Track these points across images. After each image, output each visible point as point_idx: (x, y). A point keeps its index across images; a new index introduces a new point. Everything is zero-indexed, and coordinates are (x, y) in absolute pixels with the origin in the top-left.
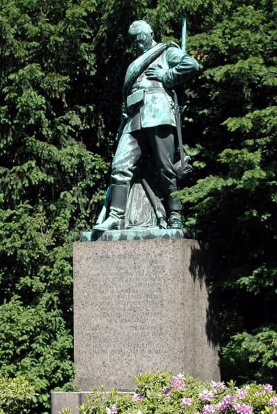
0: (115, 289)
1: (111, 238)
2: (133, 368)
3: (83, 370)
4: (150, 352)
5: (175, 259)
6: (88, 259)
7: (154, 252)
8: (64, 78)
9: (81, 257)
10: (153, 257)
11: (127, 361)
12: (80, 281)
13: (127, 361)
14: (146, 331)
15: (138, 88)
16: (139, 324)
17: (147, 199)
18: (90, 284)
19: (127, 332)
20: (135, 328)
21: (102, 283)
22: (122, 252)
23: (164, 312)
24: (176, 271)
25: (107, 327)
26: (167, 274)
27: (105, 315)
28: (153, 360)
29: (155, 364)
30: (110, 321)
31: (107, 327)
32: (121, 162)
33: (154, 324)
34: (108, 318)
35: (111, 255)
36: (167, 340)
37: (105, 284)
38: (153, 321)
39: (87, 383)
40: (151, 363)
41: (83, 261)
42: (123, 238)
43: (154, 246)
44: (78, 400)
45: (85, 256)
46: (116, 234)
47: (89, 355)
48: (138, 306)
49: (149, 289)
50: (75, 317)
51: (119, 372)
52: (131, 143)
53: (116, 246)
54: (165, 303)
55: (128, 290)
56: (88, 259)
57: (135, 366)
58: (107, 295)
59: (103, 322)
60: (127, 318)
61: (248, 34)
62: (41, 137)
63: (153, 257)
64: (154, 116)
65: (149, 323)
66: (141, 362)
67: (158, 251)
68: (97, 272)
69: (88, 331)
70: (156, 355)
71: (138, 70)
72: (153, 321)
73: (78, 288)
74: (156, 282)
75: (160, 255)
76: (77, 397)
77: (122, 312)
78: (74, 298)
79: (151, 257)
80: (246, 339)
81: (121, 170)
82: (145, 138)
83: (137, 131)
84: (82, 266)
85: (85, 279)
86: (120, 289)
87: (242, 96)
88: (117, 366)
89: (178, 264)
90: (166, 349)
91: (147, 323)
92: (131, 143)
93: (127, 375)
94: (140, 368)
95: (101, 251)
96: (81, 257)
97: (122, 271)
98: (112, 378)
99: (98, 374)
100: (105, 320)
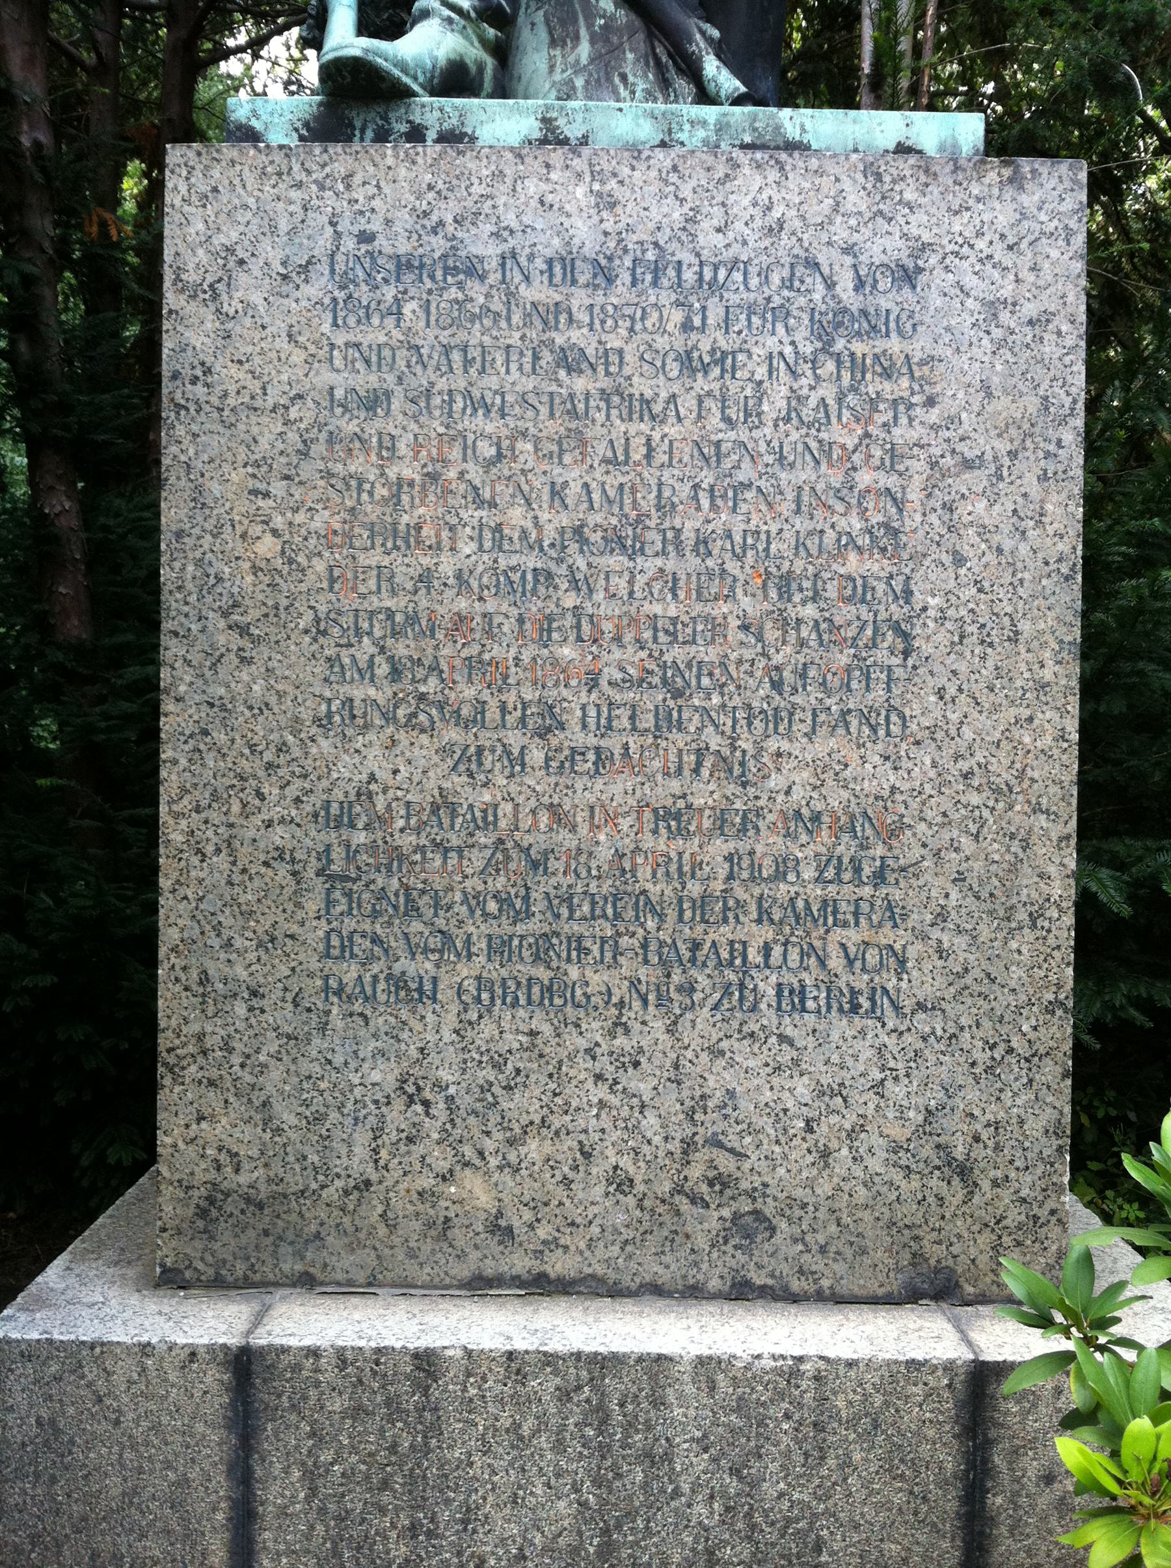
0: (517, 516)
2: (650, 1122)
3: (230, 1128)
4: (794, 999)
5: (1030, 309)
7: (848, 250)
8: (389, 152)
9: (233, 260)
11: (604, 1064)
12: (215, 444)
13: (604, 1064)
14: (768, 844)
18: (308, 470)
21: (410, 471)
22: (585, 233)
23: (923, 708)
24: (1032, 404)
25: (444, 804)
26: (953, 420)
27: (416, 714)
28: (814, 1061)
29: (839, 1091)
30: (469, 762)
31: (444, 804)
33: (837, 797)
34: (453, 734)
35: (491, 251)
36: (942, 916)
37: (433, 477)
40: (803, 1088)
41: (250, 289)
43: (855, 200)
45: (272, 252)
47: (286, 1017)
48: (711, 654)
51: (534, 1149)
53: (532, 187)
54: (932, 640)
57: (670, 1101)
58: (447, 566)
60: (613, 743)
66: (720, 1078)
69: (279, 836)
70: (840, 1027)
73: (199, 500)
74: (864, 478)
75: (907, 276)
76: (214, 1378)
77: (574, 701)
79: (830, 285)
86: (553, 521)
87: (544, 1385)
88: (524, 1104)
89: (1049, 349)
90: (925, 981)
91: (775, 781)
93: (599, 1169)
94: (711, 1123)
95: (404, 220)
96: (233, 260)
97: (580, 384)
98: (477, 1192)
99: (358, 1162)
100: (423, 749)
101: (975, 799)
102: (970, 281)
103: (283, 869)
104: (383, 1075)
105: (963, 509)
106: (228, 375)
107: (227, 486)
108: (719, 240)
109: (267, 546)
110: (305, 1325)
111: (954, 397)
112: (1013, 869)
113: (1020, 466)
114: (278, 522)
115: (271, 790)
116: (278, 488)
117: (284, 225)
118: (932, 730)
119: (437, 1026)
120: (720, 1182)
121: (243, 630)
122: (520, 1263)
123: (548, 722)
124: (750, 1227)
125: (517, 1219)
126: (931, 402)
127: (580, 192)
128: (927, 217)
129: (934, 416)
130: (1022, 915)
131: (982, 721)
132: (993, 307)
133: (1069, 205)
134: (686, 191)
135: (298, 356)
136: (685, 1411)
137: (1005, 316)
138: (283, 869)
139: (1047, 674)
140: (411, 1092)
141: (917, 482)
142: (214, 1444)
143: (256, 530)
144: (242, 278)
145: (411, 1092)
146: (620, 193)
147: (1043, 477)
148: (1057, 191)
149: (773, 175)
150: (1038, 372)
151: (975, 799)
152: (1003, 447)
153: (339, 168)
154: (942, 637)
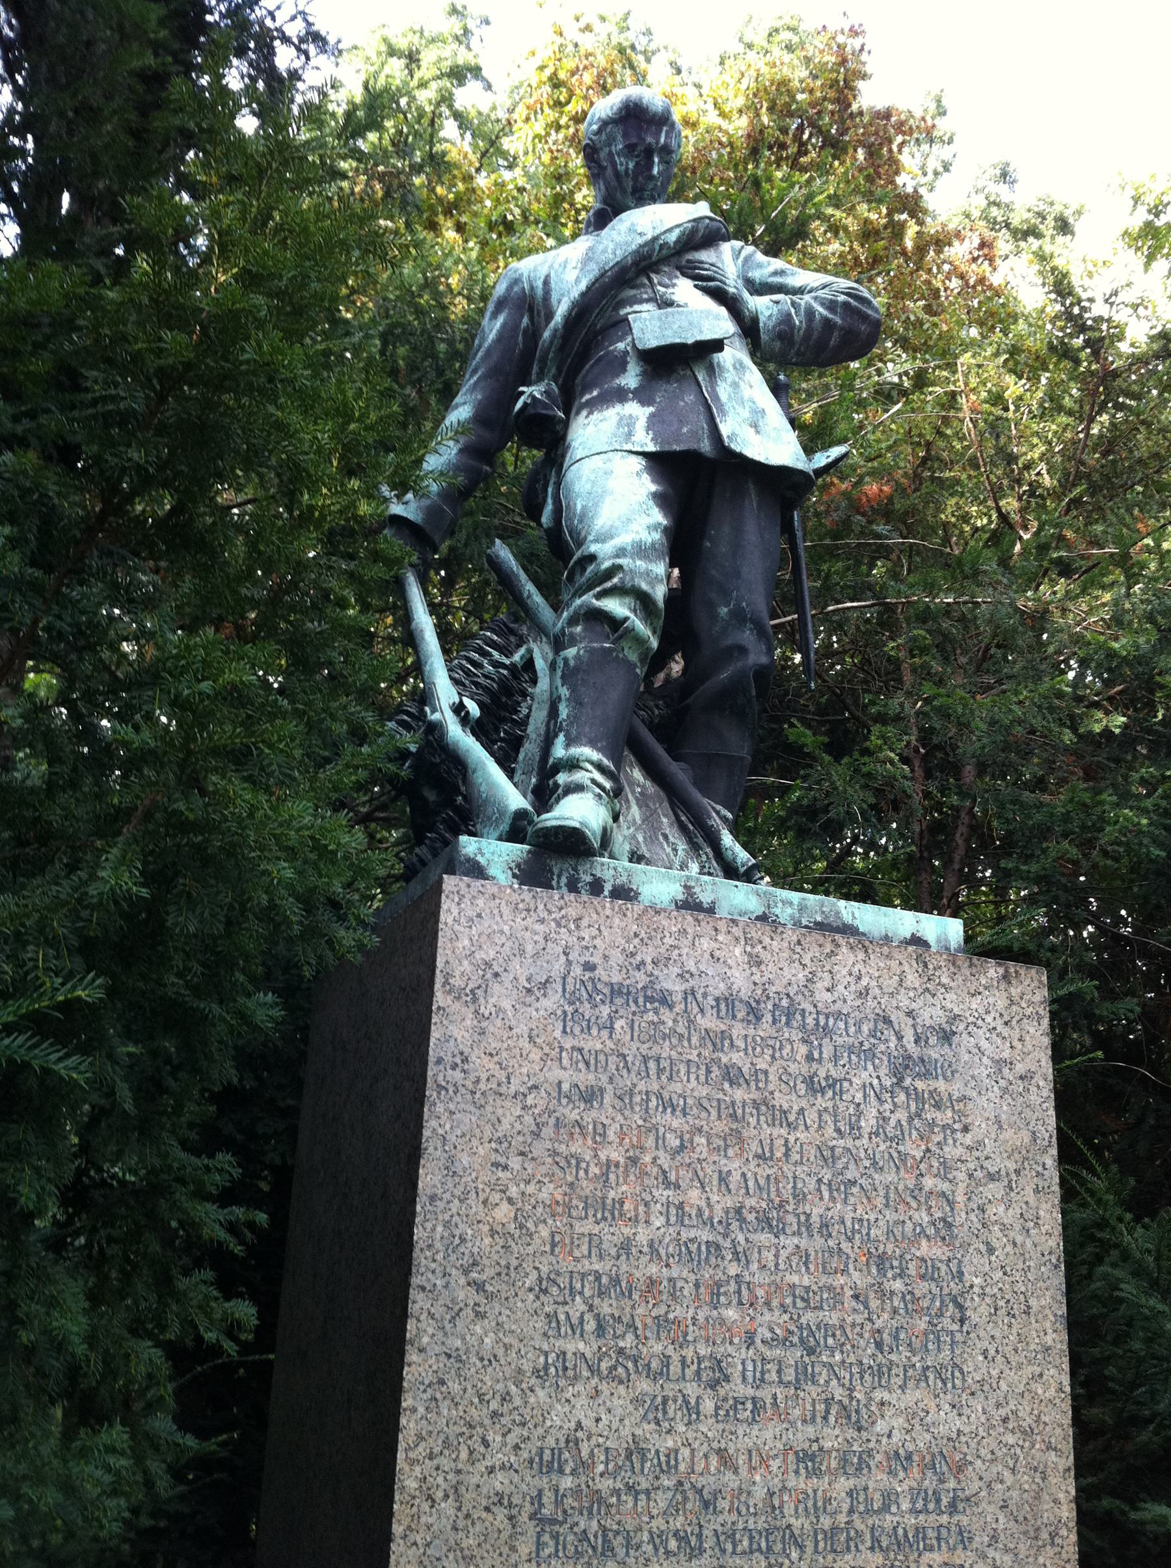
0: (694, 1196)
5: (1020, 1068)
6: (537, 988)
9: (491, 972)
10: (909, 1037)
14: (878, 1480)
16: (832, 1437)
19: (760, 1493)
23: (975, 1367)
24: (1026, 1137)
26: (980, 1144)
34: (644, 1385)
36: (994, 1538)
37: (634, 1161)
38: (915, 1417)
41: (501, 996)
43: (912, 979)
45: (520, 970)
48: (833, 1318)
49: (890, 1215)
50: (409, 1374)
53: (706, 944)
54: (978, 1312)
56: (537, 988)
58: (643, 1236)
60: (765, 1394)
63: (909, 1037)
68: (586, 1078)
69: (500, 1482)
71: (672, 237)
72: (915, 1417)
73: (450, 1169)
77: (738, 1356)
78: (1050, 1215)
80: (729, 1475)
81: (644, 586)
83: (691, 456)
84: (494, 1027)
85: (509, 1115)
86: (722, 1203)
89: (1034, 1098)
91: (880, 1427)
95: (617, 957)
96: (491, 972)
97: (739, 1094)
100: (619, 1399)
101: (1011, 1439)
102: (984, 1044)
103: (501, 1513)
105: (991, 1210)
106: (480, 1064)
107: (474, 1158)
108: (828, 997)
109: (504, 1212)
112: (1037, 1497)
113: (1022, 1181)
114: (513, 1191)
115: (495, 1438)
116: (515, 1162)
117: (530, 949)
118: (981, 1382)
121: (479, 1287)
126: (966, 1129)
127: (738, 951)
129: (968, 1139)
130: (1045, 1535)
131: (1011, 1375)
132: (1000, 1063)
133: (1038, 998)
134: (806, 961)
135: (536, 1055)
137: (1006, 1071)
138: (501, 1513)
139: (1049, 1340)
141: (961, 1188)
143: (495, 1197)
144: (496, 988)
146: (765, 956)
147: (1037, 1191)
149: (861, 955)
150: (1028, 1113)
151: (1011, 1439)
152: (1012, 1166)
153: (572, 912)
154: (984, 1310)
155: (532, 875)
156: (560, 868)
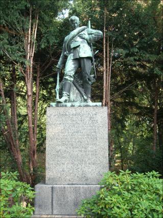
1: (66, 106)
9: (51, 115)
15: (76, 41)
16: (83, 149)
17: (77, 91)
20: (81, 151)
22: (74, 112)
25: (65, 151)
27: (63, 145)
31: (65, 151)
32: (70, 71)
33: (92, 150)
39: (53, 180)
41: (52, 116)
42: (72, 106)
44: (51, 190)
46: (69, 104)
52: (73, 64)
54: (98, 139)
55: (77, 132)
59: (63, 148)
61: (24, 146)
62: (115, 186)
64: (84, 53)
65: (89, 149)
67: (94, 113)
77: (74, 144)
82: (79, 61)
90: (99, 162)
92: (73, 64)
96: (51, 115)
99: (59, 175)
104: (61, 170)
106: (51, 122)
110: (54, 186)
111: (99, 122)
119: (65, 166)
120: (85, 176)
122: (71, 183)
123: (72, 145)
124: (87, 180)
125: (71, 179)
128: (97, 110)
136: (82, 190)
140: (63, 171)
142: (51, 193)
145: (63, 171)
148: (105, 109)
155: (57, 106)
156: (60, 104)
